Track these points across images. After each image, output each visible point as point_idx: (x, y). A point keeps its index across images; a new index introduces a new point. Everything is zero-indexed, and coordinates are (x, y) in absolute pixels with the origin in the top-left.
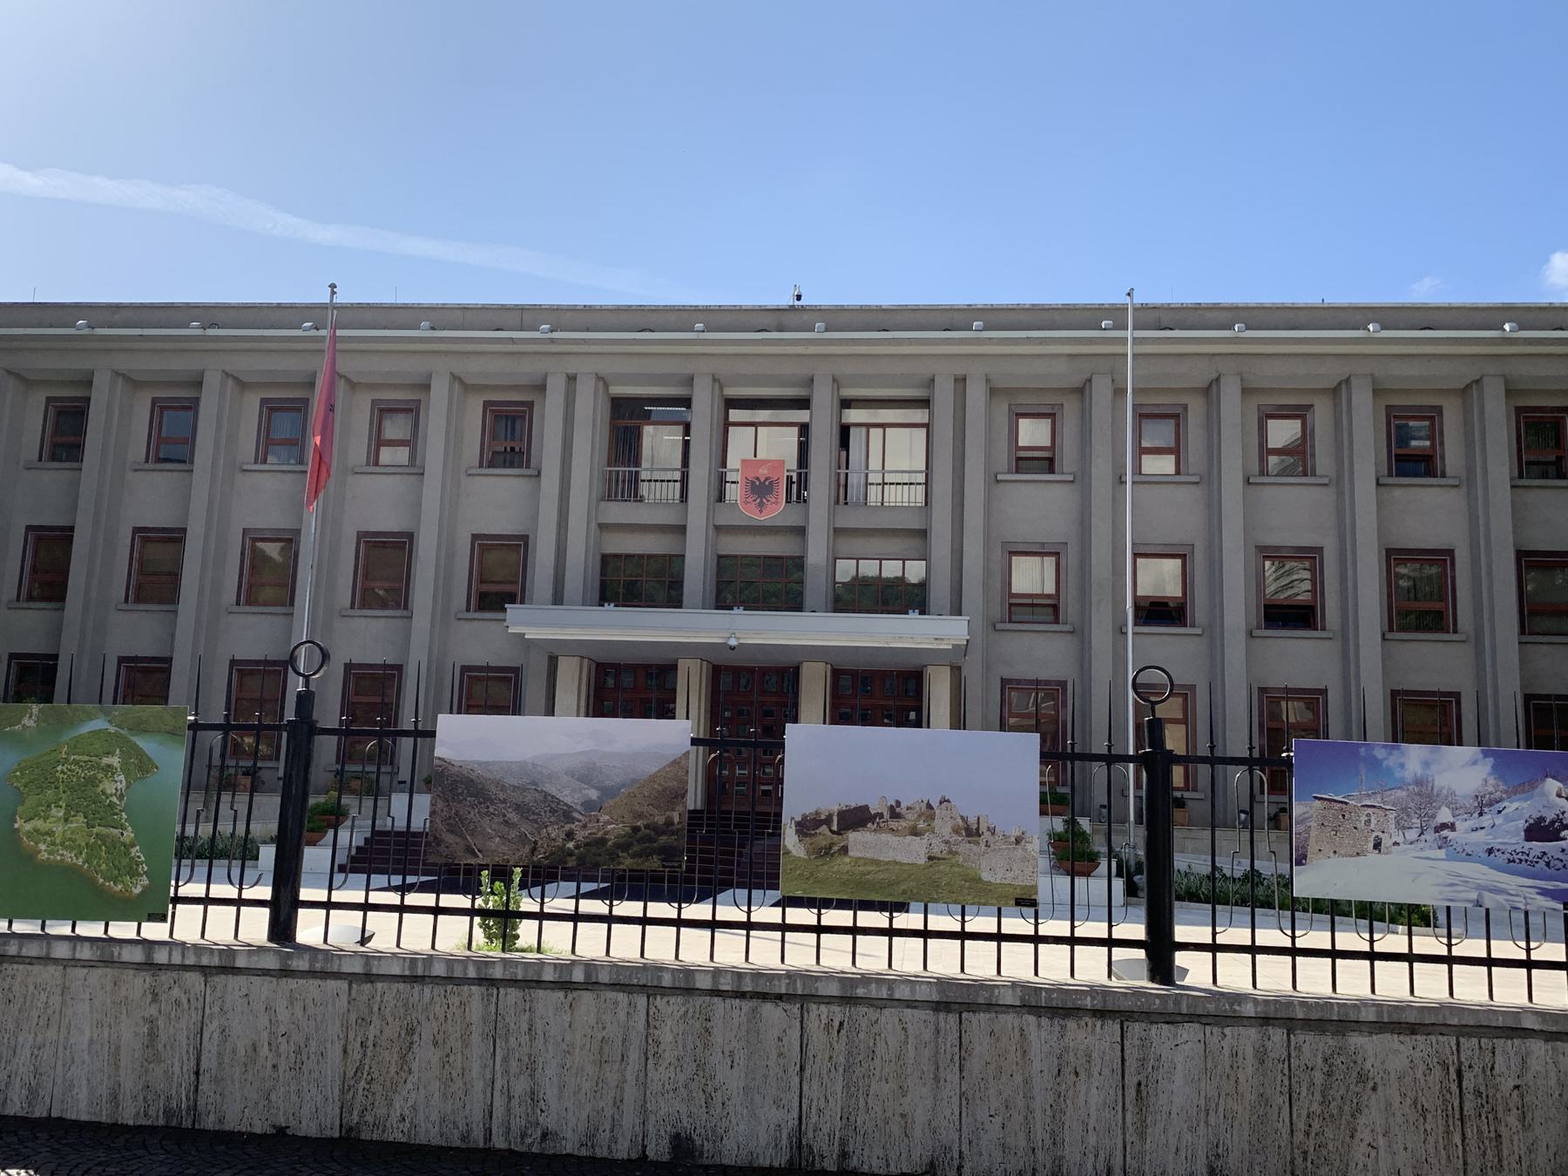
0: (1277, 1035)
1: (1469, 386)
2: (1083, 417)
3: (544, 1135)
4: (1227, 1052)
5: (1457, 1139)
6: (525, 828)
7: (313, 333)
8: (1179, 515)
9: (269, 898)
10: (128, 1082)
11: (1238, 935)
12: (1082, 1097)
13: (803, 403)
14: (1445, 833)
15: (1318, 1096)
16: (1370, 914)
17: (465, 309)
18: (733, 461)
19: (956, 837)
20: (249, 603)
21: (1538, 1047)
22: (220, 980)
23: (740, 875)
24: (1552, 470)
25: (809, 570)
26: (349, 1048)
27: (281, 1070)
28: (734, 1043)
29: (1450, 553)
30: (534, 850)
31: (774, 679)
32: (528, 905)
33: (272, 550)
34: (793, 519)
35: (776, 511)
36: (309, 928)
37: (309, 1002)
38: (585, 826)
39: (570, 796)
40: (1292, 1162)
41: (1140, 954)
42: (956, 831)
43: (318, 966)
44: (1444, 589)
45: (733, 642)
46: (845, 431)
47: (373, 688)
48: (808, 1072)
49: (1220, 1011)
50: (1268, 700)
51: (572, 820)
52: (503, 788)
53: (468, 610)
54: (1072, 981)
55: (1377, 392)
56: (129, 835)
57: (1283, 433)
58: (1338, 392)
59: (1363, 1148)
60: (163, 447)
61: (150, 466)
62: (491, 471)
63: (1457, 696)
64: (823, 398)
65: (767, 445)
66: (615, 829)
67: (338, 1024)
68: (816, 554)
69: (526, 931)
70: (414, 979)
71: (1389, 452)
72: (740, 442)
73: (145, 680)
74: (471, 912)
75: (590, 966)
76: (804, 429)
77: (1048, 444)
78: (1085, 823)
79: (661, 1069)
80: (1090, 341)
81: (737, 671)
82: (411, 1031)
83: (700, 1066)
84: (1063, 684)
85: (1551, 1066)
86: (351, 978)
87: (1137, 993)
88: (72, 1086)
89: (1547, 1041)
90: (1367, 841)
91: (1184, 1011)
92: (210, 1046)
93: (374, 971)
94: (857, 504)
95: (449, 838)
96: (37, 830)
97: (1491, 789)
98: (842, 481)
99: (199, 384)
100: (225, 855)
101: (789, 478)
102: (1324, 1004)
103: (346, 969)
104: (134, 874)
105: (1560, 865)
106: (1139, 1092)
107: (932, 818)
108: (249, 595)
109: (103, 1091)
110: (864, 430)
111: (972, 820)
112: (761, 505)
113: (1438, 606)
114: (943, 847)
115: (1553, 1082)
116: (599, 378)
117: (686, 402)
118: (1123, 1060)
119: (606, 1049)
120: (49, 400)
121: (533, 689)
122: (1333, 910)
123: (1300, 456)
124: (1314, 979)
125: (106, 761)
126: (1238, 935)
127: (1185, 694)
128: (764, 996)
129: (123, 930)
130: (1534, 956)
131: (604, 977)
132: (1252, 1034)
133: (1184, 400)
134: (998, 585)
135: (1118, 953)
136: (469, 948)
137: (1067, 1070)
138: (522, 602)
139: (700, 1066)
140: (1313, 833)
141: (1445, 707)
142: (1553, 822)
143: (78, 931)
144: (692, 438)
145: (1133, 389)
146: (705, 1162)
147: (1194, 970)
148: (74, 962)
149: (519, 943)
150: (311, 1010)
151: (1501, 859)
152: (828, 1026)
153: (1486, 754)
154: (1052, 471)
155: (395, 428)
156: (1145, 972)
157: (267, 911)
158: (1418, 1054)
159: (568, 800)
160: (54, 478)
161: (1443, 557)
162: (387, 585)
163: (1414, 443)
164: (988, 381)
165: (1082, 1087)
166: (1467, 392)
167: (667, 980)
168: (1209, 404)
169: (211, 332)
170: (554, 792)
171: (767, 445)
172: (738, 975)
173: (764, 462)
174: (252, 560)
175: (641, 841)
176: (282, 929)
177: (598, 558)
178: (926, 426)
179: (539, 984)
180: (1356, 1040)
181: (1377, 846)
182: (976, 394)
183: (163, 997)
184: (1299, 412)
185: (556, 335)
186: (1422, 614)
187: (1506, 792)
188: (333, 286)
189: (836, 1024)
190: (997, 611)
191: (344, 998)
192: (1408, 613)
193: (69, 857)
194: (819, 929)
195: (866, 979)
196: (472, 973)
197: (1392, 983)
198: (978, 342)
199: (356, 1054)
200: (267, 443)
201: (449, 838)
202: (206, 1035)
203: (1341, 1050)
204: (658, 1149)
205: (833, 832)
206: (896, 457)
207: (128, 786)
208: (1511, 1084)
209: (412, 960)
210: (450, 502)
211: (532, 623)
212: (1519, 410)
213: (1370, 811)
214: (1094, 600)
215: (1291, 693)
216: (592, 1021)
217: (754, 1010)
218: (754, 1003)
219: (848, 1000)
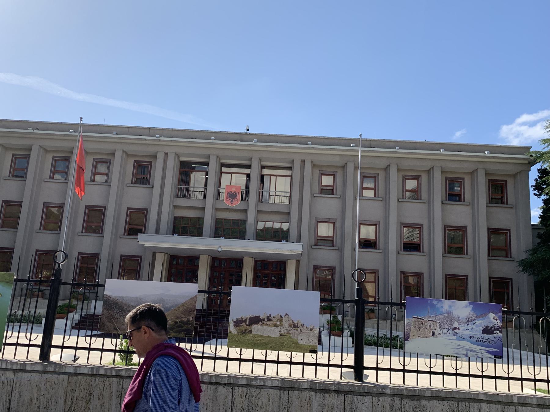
0: (397, 400)
1: (473, 172)
2: (344, 175)
4: (380, 406)
7: (74, 133)
8: (375, 211)
13: (248, 166)
14: (456, 331)
19: (290, 328)
21: (484, 406)
22: (19, 374)
24: (500, 201)
26: (67, 400)
27: (41, 408)
28: (208, 400)
29: (466, 228)
33: (54, 210)
34: (243, 206)
35: (237, 204)
36: (55, 356)
37: (53, 383)
41: (352, 370)
42: (290, 326)
43: (57, 370)
44: (463, 240)
45: (220, 250)
46: (262, 177)
49: (379, 392)
50: (404, 276)
53: (124, 235)
54: (328, 380)
55: (443, 172)
57: (411, 184)
58: (387, 169)
60: (15, 172)
62: (136, 185)
63: (422, 274)
64: (255, 165)
65: (235, 180)
67: (63, 391)
68: (251, 218)
70: (92, 375)
71: (446, 193)
72: (225, 179)
76: (248, 176)
77: (332, 185)
78: (340, 318)
80: (347, 150)
81: (220, 260)
82: (90, 394)
84: (334, 268)
86: (69, 374)
87: (350, 385)
89: (487, 404)
90: (430, 333)
91: (366, 391)
93: (78, 372)
94: (266, 202)
95: (108, 324)
97: (471, 316)
98: (261, 194)
100: (27, 322)
101: (242, 192)
102: (413, 390)
103: (67, 371)
105: (493, 342)
107: (282, 321)
110: (269, 177)
111: (296, 322)
112: (232, 201)
114: (285, 331)
116: (176, 154)
117: (207, 164)
118: (344, 408)
123: (416, 193)
127: (375, 273)
128: (219, 384)
132: (389, 399)
134: (313, 233)
136: (114, 364)
138: (144, 233)
142: (491, 328)
144: (208, 177)
147: (370, 377)
149: (133, 362)
150: (54, 386)
151: (474, 340)
152: (242, 395)
153: (470, 304)
154: (333, 194)
155: (102, 168)
157: (39, 349)
163: (456, 188)
164: (312, 162)
166: (472, 173)
168: (386, 173)
171: (235, 180)
172: (210, 376)
173: (233, 186)
174: (47, 212)
175: (178, 327)
176: (45, 355)
177: (173, 217)
178: (291, 176)
180: (424, 402)
181: (433, 334)
182: (308, 166)
184: (416, 178)
185: (161, 138)
187: (476, 317)
188: (81, 118)
189: (245, 394)
190: (312, 241)
191: (66, 382)
192: (451, 248)
195: (256, 378)
196: (114, 374)
198: (309, 148)
199: (69, 403)
200: (54, 171)
201: (108, 324)
202: (13, 395)
203: (419, 406)
205: (247, 325)
206: (280, 187)
209: (92, 368)
210: (119, 196)
211: (148, 240)
212: (489, 180)
213: (431, 322)
214: (346, 239)
215: (413, 274)
217: (215, 389)
219: (249, 386)
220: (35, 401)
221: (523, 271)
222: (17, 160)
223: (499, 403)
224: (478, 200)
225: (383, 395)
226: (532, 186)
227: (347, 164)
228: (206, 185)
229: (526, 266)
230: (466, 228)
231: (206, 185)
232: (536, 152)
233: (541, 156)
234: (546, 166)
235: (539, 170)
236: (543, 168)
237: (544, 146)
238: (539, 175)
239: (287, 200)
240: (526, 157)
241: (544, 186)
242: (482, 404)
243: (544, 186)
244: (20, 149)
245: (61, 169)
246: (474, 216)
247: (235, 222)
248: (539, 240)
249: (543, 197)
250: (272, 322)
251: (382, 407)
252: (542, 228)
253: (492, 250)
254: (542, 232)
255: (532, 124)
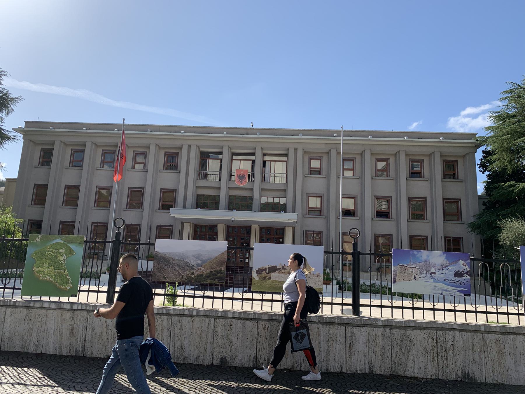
0: (388, 330)
1: (431, 154)
3: (184, 358)
5: (436, 359)
6: (180, 271)
7: (118, 132)
8: (354, 187)
9: (106, 290)
10: (65, 343)
11: (377, 302)
12: (335, 347)
13: (253, 154)
14: (433, 275)
15: (399, 347)
16: (412, 296)
17: (160, 126)
18: (234, 169)
20: (98, 206)
21: (458, 333)
23: (240, 284)
24: (452, 177)
25: (254, 201)
30: (182, 278)
31: (244, 229)
32: (179, 292)
33: (104, 192)
35: (246, 184)
38: (197, 271)
39: (193, 263)
40: (392, 365)
41: (351, 307)
44: (423, 208)
45: (233, 219)
46: (264, 163)
47: (133, 230)
48: (259, 341)
49: (372, 323)
51: (193, 269)
52: (174, 260)
56: (66, 272)
57: (381, 165)
58: (396, 155)
59: (411, 361)
61: (70, 168)
64: (259, 153)
66: (205, 271)
68: (256, 195)
69: (179, 301)
72: (236, 164)
73: (67, 228)
74: (165, 295)
75: (198, 310)
76: (253, 162)
79: (218, 339)
80: (331, 140)
81: (234, 227)
83: (229, 338)
85: (461, 339)
87: (350, 318)
88: (48, 344)
92: (89, 332)
95: (159, 274)
96: (39, 271)
99: (85, 145)
102: (400, 322)
104: (67, 283)
106: (350, 346)
108: (97, 204)
109: (57, 346)
112: (241, 182)
113: (422, 213)
115: (461, 343)
116: (197, 146)
119: (202, 333)
120: (42, 149)
121: (176, 232)
122: (403, 296)
124: (397, 315)
125: (60, 251)
126: (377, 302)
128: (247, 319)
129: (64, 299)
130: (478, 310)
131: (202, 314)
133: (355, 156)
135: (345, 307)
137: (330, 340)
139: (229, 338)
140: (397, 275)
141: (423, 240)
143: (61, 300)
144: (223, 163)
145: (343, 153)
146: (230, 365)
147: (365, 312)
148: (50, 309)
149: (177, 304)
151: (448, 282)
152: (265, 327)
154: (320, 174)
155: (140, 159)
156: (352, 313)
157: (106, 294)
158: (425, 335)
159: (192, 264)
160: (43, 171)
161: (423, 200)
162: (136, 202)
165: (334, 344)
166: (430, 155)
167: (220, 315)
168: (362, 157)
169: (57, 130)
170: (188, 261)
172: (240, 313)
173: (242, 170)
175: (213, 275)
179: (184, 315)
180: (409, 331)
181: (415, 278)
182: (300, 153)
183: (75, 319)
184: (386, 160)
185: (185, 134)
186: (417, 215)
188: (124, 119)
189: (267, 327)
190: (304, 212)
193: (49, 278)
194: (262, 300)
196: (164, 312)
197: (418, 316)
198: (370, 140)
200: (104, 162)
204: (217, 362)
206: (278, 170)
207: (67, 258)
208: (451, 343)
210: (155, 179)
212: (444, 161)
215: (381, 235)
216: (198, 326)
217: (244, 323)
218: (244, 321)
220: (105, 334)
221: (471, 231)
222: (75, 153)
223: (470, 331)
224: (435, 177)
225: (377, 326)
226: (478, 164)
227: (330, 150)
228: (221, 170)
229: (474, 227)
230: (426, 198)
231: (221, 170)
232: (481, 137)
233: (485, 140)
234: (489, 148)
235: (483, 151)
236: (487, 150)
237: (487, 132)
238: (484, 155)
239: (284, 180)
240: (473, 141)
241: (488, 164)
242: (455, 332)
243: (488, 164)
244: (77, 145)
245: (109, 160)
246: (432, 189)
247: (244, 198)
248: (484, 207)
249: (487, 173)
250: (286, 271)
251: (376, 336)
252: (487, 197)
253: (447, 216)
254: (486, 201)
255: (475, 116)
